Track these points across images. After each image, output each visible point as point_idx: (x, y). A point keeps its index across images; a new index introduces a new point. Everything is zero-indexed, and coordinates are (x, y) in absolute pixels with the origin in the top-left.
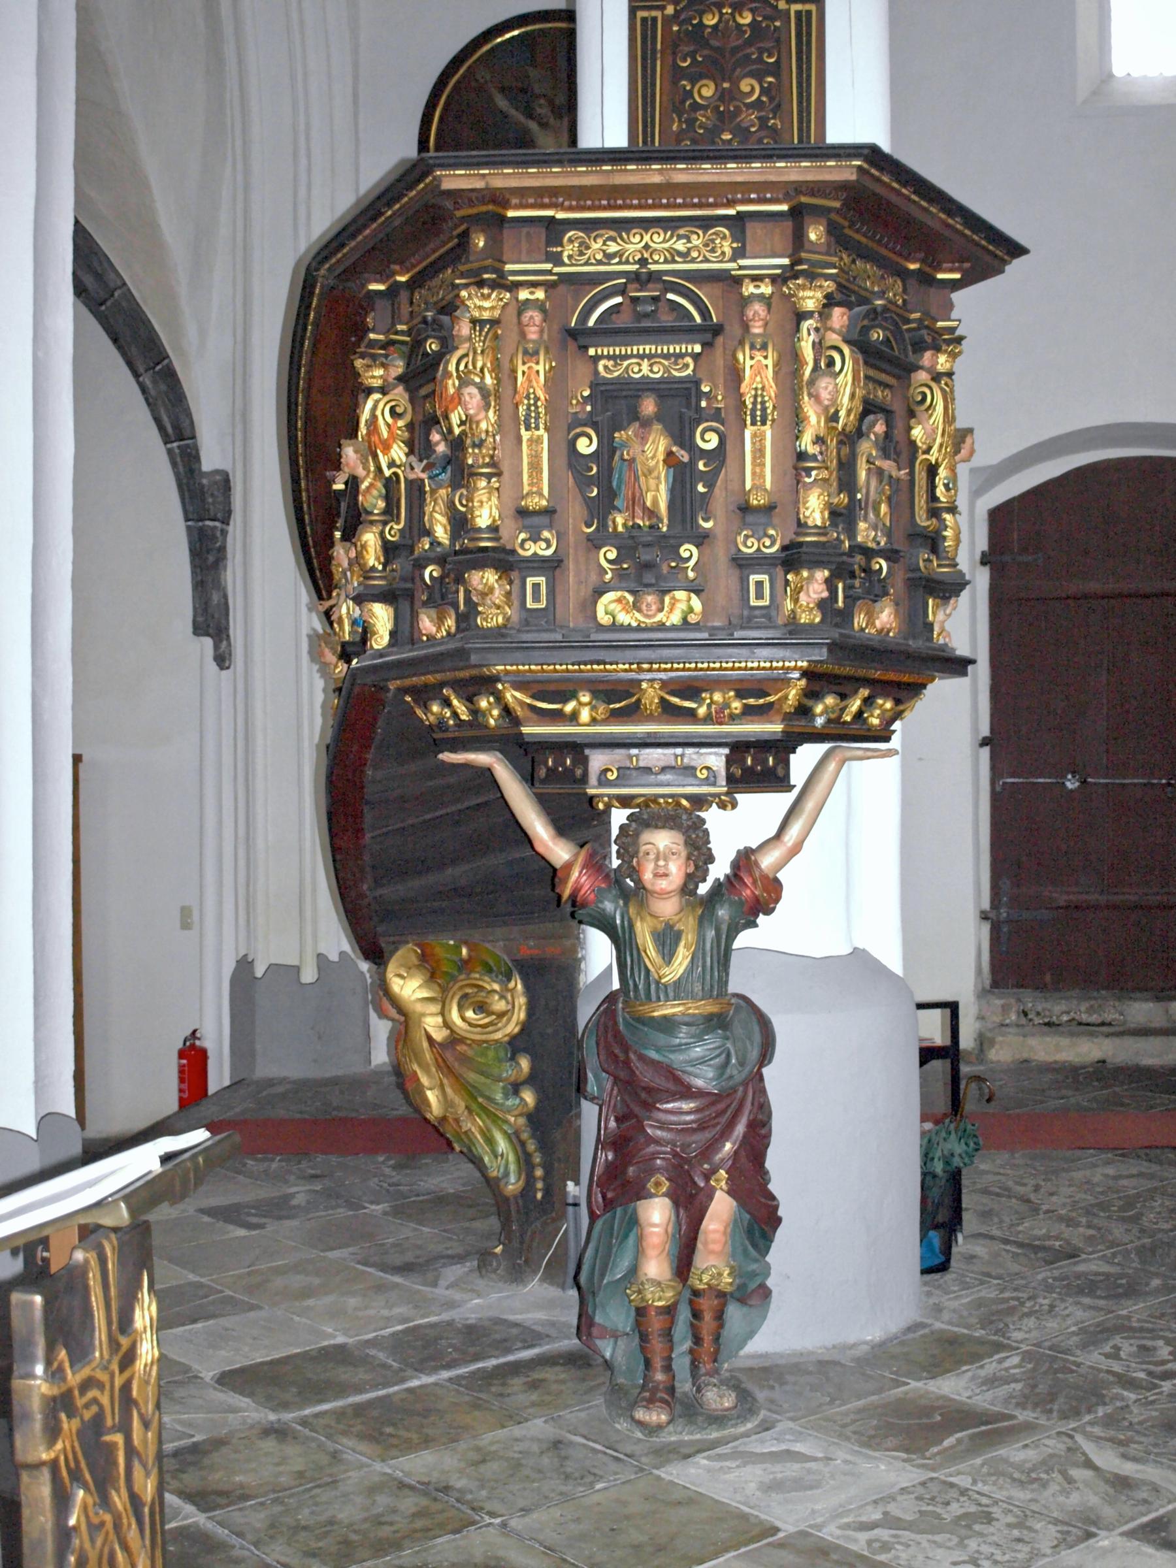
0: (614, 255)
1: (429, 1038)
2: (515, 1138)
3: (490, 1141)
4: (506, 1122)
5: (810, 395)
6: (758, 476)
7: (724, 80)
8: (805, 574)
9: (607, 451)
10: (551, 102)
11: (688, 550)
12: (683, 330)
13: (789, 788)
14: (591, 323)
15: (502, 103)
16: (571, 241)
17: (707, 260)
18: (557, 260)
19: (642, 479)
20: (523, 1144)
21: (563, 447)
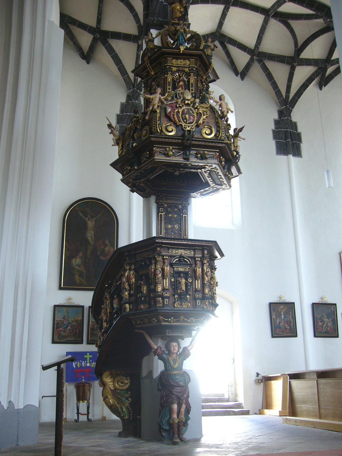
0: (177, 253)
1: (111, 389)
2: (127, 408)
3: (122, 409)
4: (126, 405)
5: (206, 275)
6: (198, 286)
7: (172, 225)
8: (206, 300)
9: (176, 281)
10: (91, 215)
11: (188, 296)
12: (187, 264)
13: (192, 337)
14: (174, 262)
15: (81, 214)
16: (170, 250)
17: (190, 254)
18: (168, 252)
19: (182, 286)
20: (128, 409)
21: (170, 280)
